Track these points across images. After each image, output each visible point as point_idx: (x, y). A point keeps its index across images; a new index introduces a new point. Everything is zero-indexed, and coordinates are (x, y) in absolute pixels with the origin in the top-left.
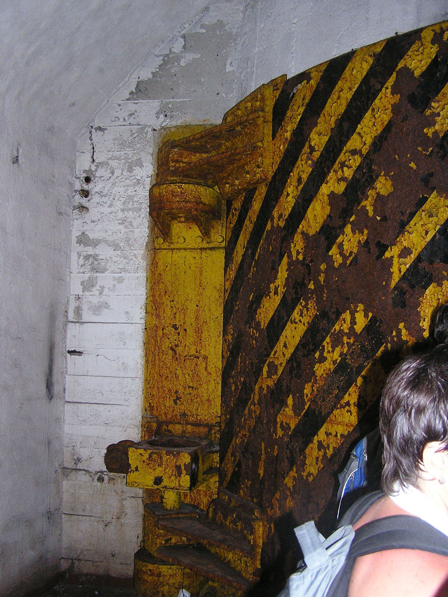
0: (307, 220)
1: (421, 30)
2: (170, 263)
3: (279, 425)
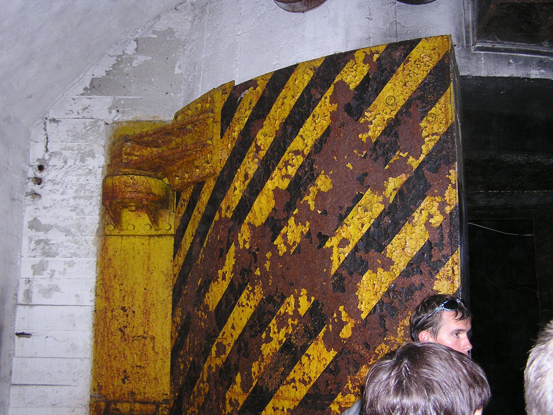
0: (254, 212)
1: (354, 51)
2: (120, 249)
3: (227, 402)
